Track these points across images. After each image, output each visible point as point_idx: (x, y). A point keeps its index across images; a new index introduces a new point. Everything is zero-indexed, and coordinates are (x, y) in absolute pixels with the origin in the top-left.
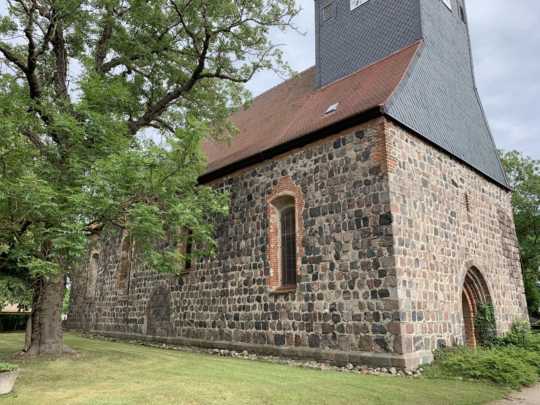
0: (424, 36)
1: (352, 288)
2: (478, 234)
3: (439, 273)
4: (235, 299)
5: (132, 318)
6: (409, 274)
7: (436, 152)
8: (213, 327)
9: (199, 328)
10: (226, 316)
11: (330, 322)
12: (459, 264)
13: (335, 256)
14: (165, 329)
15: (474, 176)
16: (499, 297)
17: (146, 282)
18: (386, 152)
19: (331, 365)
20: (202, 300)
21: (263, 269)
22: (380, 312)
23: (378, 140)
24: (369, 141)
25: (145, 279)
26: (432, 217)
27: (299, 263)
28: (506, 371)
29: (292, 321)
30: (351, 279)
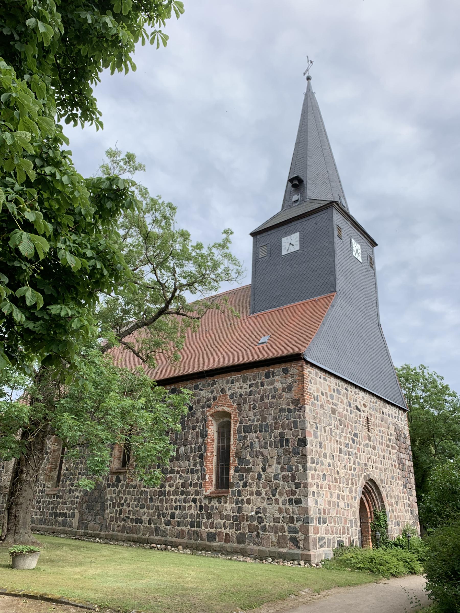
0: (337, 290)
1: (274, 495)
2: (376, 451)
3: (341, 485)
4: (172, 499)
5: (62, 511)
6: (318, 486)
7: (343, 384)
8: (150, 524)
9: (134, 524)
10: (163, 514)
11: (255, 523)
12: (359, 477)
13: (262, 469)
14: (98, 524)
15: (375, 401)
16: (392, 505)
17: (80, 476)
18: (304, 388)
19: (255, 559)
20: (139, 498)
21: (199, 474)
22: (295, 516)
23: (299, 378)
24: (292, 377)
25: (79, 474)
26: (338, 439)
27: (232, 471)
28: (381, 565)
29: (223, 521)
30: (274, 488)
